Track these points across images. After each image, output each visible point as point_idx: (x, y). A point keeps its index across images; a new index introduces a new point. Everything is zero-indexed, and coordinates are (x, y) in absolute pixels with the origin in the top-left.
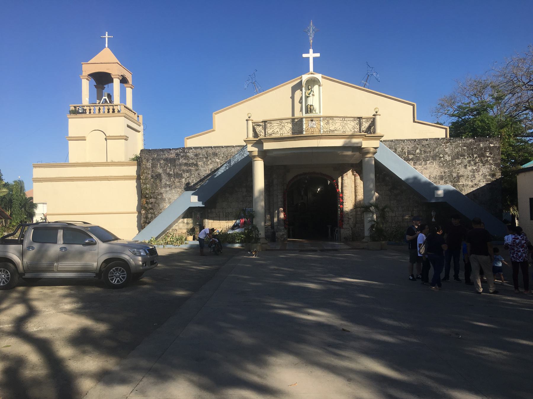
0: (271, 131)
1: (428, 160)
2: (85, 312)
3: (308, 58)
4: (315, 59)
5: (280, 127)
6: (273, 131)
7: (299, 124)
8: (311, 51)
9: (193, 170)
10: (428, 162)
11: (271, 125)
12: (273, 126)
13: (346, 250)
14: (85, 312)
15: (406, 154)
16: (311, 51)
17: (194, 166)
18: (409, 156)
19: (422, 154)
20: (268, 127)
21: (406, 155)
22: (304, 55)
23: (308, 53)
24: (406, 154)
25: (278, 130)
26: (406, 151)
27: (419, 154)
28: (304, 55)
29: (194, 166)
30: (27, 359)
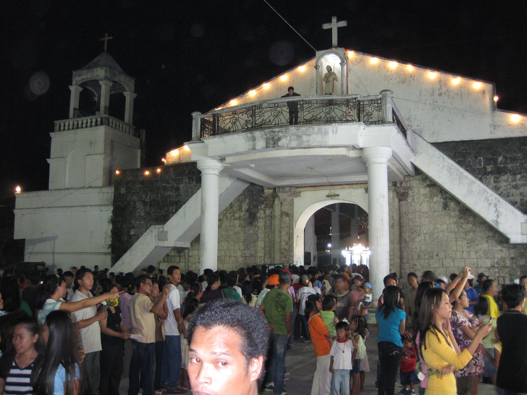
0: (261, 120)
1: (518, 174)
2: (51, 370)
3: (330, 30)
4: (340, 29)
5: (275, 114)
6: (263, 120)
7: (306, 109)
8: (334, 20)
9: (173, 195)
10: (519, 176)
11: (261, 110)
12: (263, 112)
13: (178, 391)
14: (51, 370)
15: (482, 163)
16: (334, 20)
17: (174, 191)
18: (487, 167)
19: (508, 164)
20: (256, 114)
21: (481, 165)
22: (326, 26)
23: (330, 21)
24: (482, 163)
25: (272, 118)
26: (482, 159)
27: (502, 164)
28: (326, 26)
29: (174, 191)
30: (394, 311)
